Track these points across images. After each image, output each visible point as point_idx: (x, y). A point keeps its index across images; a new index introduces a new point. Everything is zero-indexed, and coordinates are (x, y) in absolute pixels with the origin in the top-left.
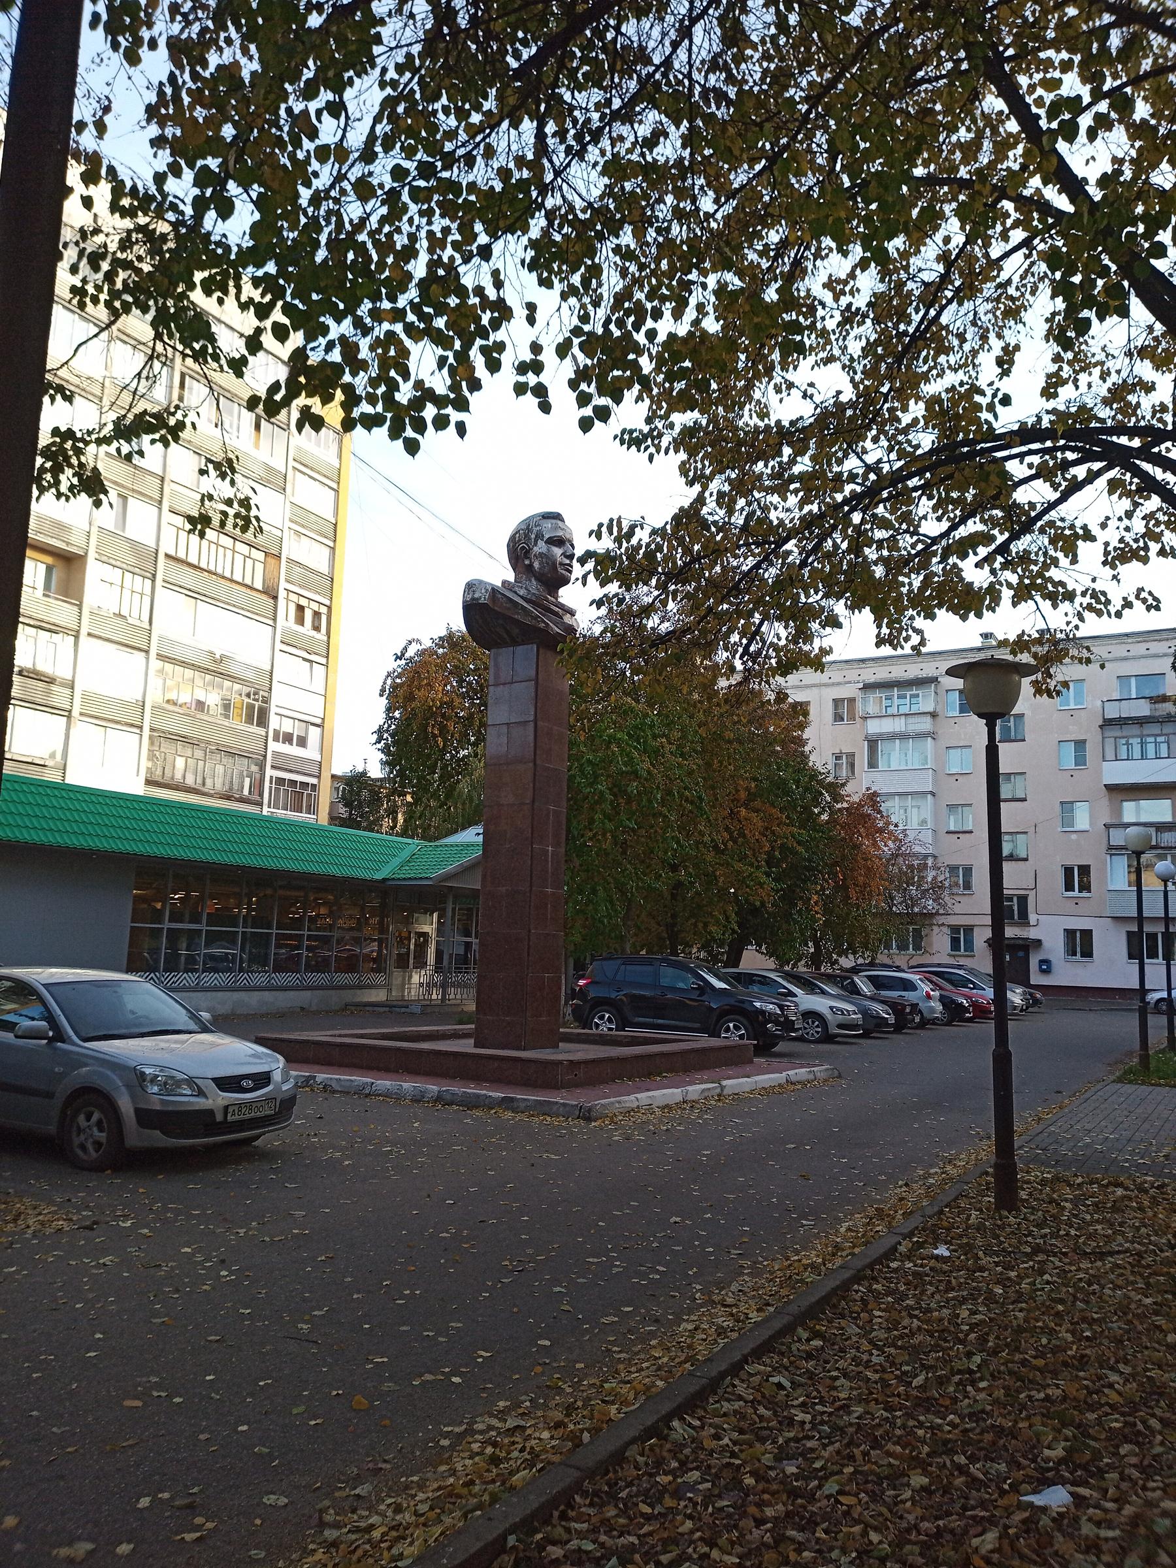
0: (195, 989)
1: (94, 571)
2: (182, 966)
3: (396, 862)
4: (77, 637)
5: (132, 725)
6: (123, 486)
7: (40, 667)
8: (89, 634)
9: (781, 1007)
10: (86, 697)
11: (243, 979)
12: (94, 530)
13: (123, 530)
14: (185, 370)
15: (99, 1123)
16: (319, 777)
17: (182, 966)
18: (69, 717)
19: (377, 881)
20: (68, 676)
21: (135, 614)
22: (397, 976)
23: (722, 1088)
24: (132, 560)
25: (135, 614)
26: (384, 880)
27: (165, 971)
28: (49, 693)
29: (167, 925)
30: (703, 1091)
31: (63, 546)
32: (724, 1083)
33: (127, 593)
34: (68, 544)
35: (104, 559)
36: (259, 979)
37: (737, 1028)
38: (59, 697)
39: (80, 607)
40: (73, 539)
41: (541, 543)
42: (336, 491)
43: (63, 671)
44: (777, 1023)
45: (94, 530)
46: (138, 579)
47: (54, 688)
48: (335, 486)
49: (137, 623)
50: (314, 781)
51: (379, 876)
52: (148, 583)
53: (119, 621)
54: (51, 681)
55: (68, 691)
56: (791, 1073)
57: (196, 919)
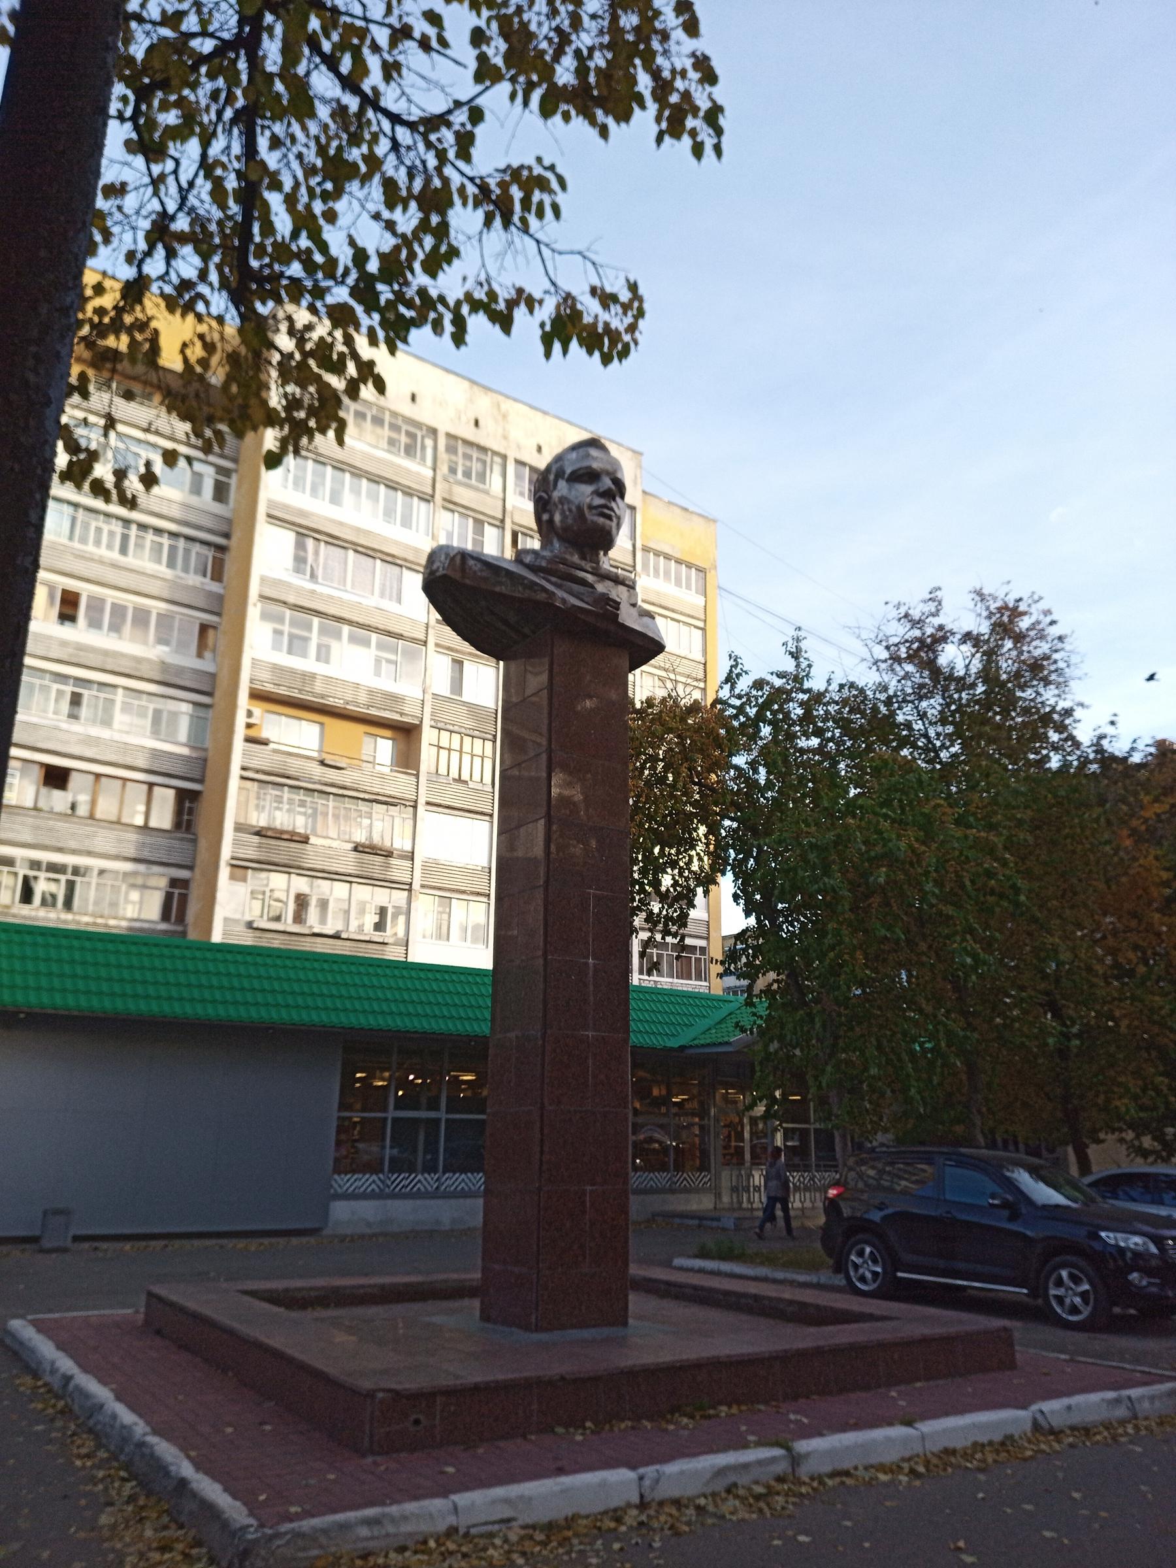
0: (436, 1195)
1: (428, 735)
2: (419, 1166)
3: (704, 1023)
4: (415, 807)
5: (478, 894)
6: (457, 651)
7: (376, 840)
8: (428, 803)
9: (1159, 1241)
10: (428, 867)
11: (401, 1180)
12: (428, 697)
13: (460, 694)
14: (517, 528)
15: (1072, 1277)
16: (707, 939)
17: (419, 1166)
18: (410, 890)
19: (671, 1049)
20: (408, 847)
21: (477, 777)
22: (727, 1178)
23: (796, 1460)
24: (469, 723)
25: (477, 777)
26: (682, 1048)
27: (392, 1171)
28: (387, 866)
29: (392, 1113)
30: (721, 1472)
31: (397, 717)
32: (803, 1446)
33: (466, 759)
34: (402, 714)
35: (440, 725)
36: (425, 1181)
37: (1075, 1279)
38: (399, 870)
39: (417, 776)
40: (407, 710)
41: (562, 484)
42: (703, 630)
43: (401, 843)
44: (1147, 1272)
45: (428, 697)
46: (478, 743)
47: (393, 861)
48: (701, 624)
49: (479, 787)
50: (703, 943)
51: (673, 1043)
52: (489, 745)
53: (460, 786)
54: (389, 854)
55: (408, 864)
56: (1052, 1406)
57: (433, 1105)
